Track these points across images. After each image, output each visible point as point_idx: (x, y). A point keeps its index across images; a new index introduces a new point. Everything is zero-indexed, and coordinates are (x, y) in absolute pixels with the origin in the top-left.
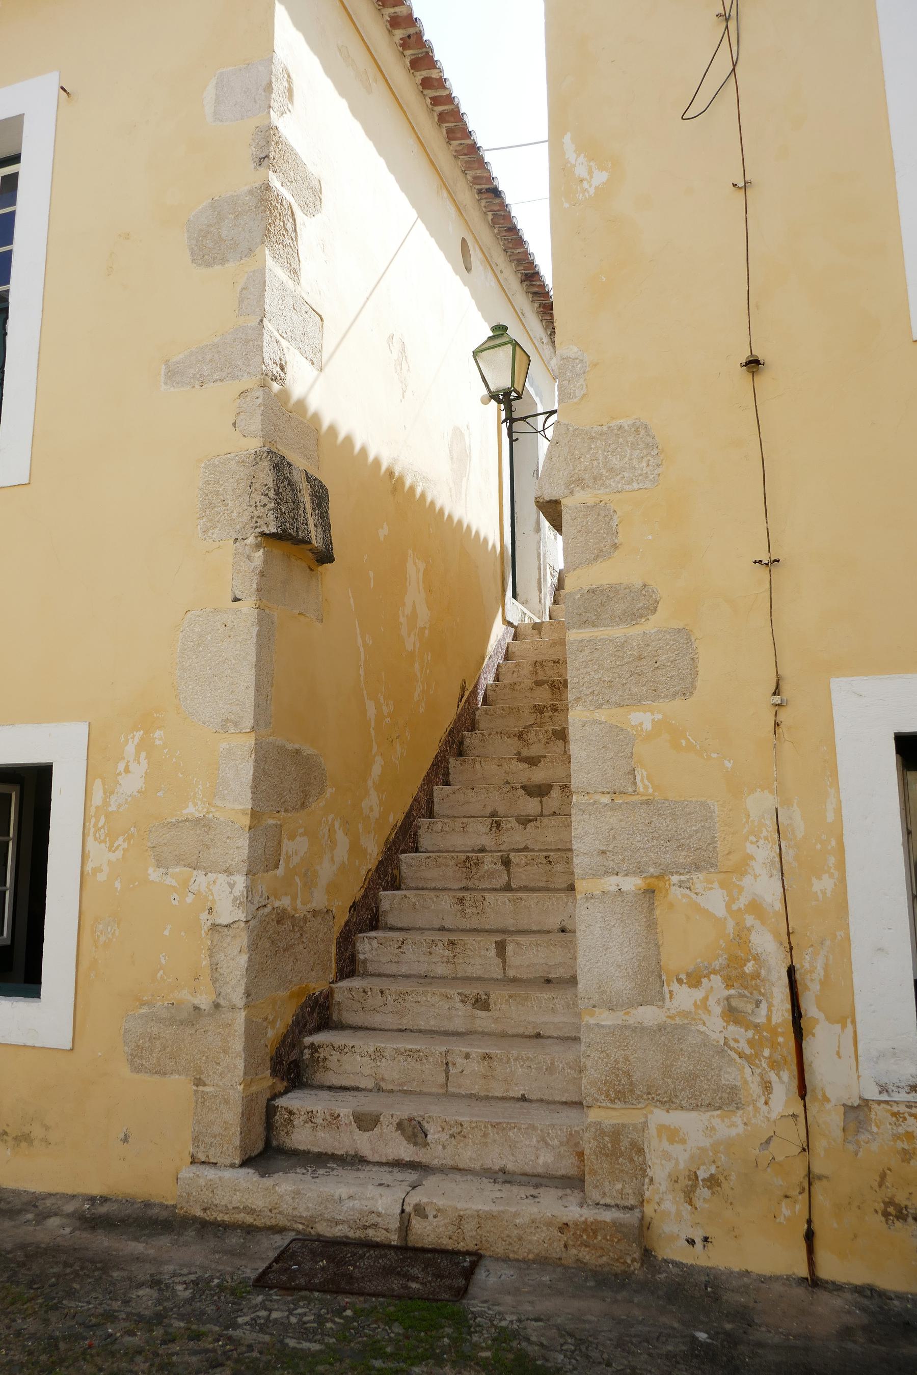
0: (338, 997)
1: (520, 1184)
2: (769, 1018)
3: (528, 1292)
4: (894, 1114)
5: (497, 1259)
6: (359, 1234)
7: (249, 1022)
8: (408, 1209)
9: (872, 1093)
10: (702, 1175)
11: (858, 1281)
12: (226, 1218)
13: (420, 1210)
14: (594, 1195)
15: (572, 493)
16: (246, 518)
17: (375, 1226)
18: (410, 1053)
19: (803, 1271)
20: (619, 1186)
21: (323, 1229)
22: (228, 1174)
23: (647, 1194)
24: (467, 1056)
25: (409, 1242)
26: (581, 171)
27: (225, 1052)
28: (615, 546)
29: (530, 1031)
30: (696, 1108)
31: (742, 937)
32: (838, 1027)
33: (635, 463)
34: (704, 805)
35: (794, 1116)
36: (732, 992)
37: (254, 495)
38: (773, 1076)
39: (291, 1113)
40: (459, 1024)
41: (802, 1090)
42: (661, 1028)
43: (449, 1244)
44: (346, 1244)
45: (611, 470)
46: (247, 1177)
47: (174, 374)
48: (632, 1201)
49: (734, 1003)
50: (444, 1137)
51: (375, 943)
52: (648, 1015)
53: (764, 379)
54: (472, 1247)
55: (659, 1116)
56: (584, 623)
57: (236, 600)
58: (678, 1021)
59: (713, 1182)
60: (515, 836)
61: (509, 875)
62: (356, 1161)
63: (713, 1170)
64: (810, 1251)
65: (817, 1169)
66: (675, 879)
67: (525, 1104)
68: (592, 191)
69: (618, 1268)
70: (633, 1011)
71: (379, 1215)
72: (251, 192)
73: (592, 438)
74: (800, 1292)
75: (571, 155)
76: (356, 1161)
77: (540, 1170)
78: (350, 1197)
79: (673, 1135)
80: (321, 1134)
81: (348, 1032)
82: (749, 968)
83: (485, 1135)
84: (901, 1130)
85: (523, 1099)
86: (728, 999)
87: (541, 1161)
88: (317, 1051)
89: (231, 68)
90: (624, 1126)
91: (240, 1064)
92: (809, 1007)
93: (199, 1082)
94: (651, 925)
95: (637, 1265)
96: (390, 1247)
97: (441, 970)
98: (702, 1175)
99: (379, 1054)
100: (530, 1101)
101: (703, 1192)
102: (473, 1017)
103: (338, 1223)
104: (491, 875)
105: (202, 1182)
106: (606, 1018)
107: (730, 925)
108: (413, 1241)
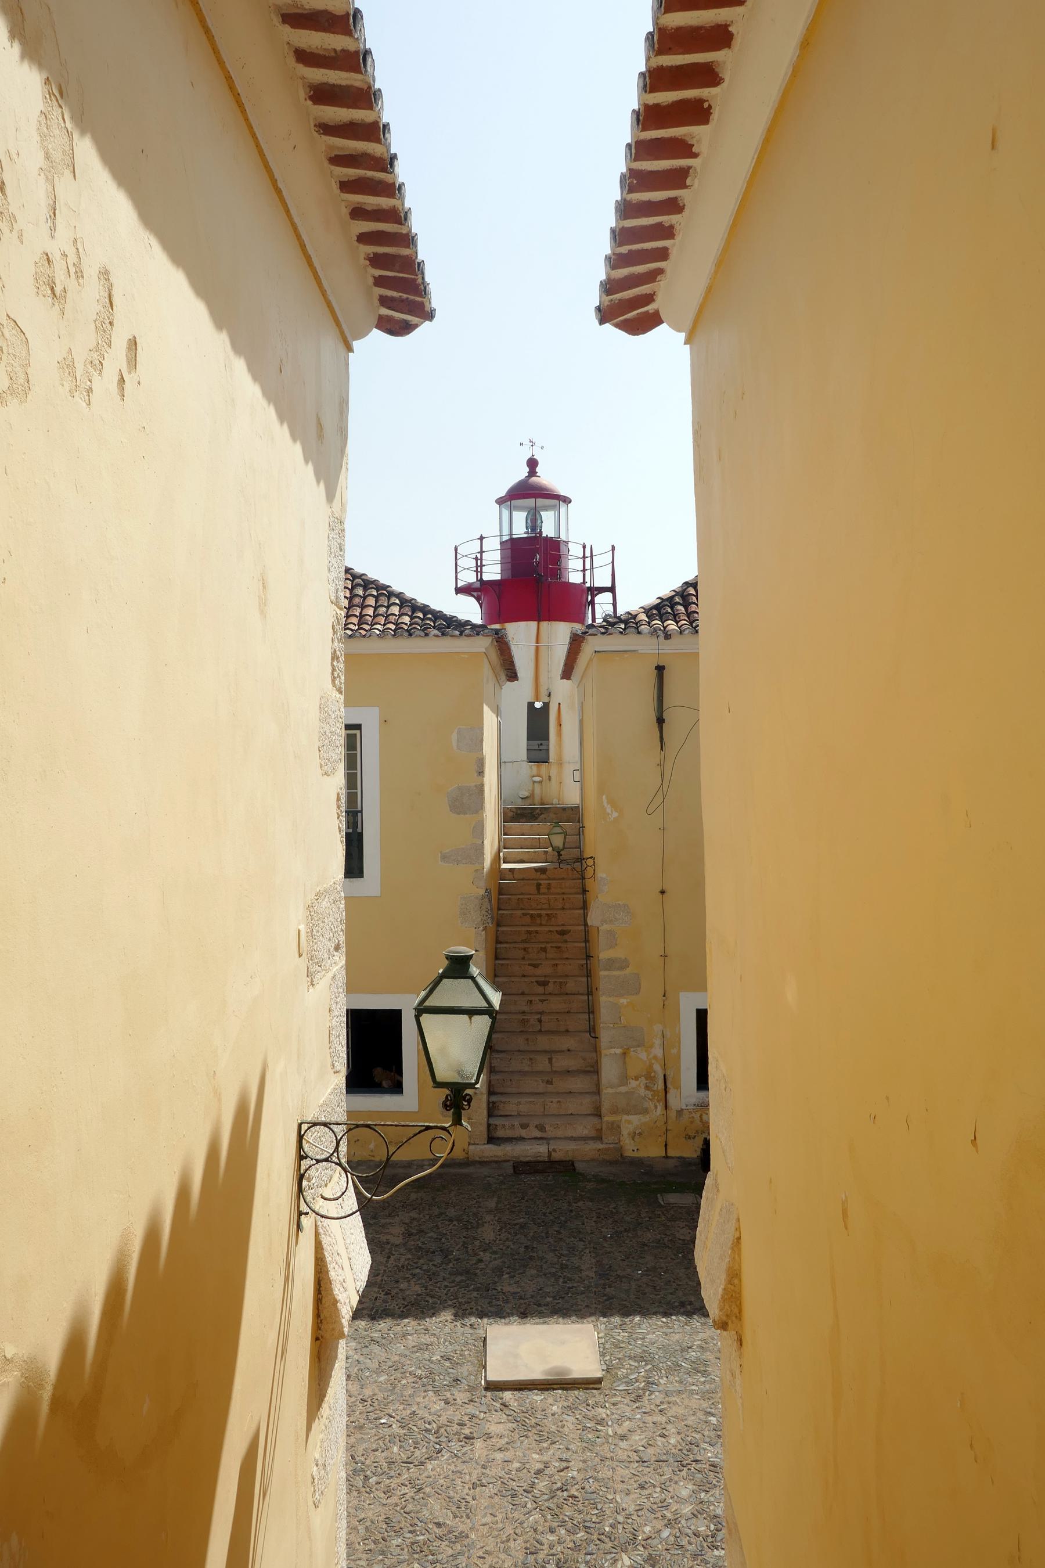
2: (657, 1088)
4: (690, 1112)
5: (579, 1161)
6: (535, 1159)
9: (684, 1107)
10: (637, 1132)
12: (488, 1160)
13: (554, 1150)
14: (605, 1140)
15: (602, 924)
16: (479, 919)
17: (540, 1156)
18: (530, 1102)
19: (664, 1155)
20: (613, 1137)
21: (522, 1159)
22: (482, 1147)
23: (621, 1139)
24: (552, 1102)
25: (551, 1158)
26: (609, 810)
28: (616, 945)
29: (568, 1091)
30: (636, 1114)
31: (651, 1066)
32: (676, 1090)
33: (624, 917)
35: (663, 1115)
36: (648, 1081)
37: (482, 911)
38: (658, 1104)
39: (496, 1126)
40: (541, 1090)
41: (666, 1107)
42: (627, 1093)
43: (564, 1159)
44: (531, 1162)
47: (445, 858)
48: (617, 1142)
49: (647, 1084)
50: (552, 1129)
51: (499, 1060)
52: (623, 1089)
53: (665, 895)
54: (571, 1158)
55: (625, 1117)
56: (606, 970)
58: (631, 1090)
59: (640, 1134)
60: (540, 1007)
61: (541, 1026)
62: (522, 1139)
63: (640, 1131)
64: (666, 1149)
65: (669, 1128)
66: (632, 1049)
67: (572, 1116)
68: (612, 819)
70: (618, 1088)
71: (541, 1153)
72: (476, 786)
75: (605, 804)
76: (522, 1139)
77: (583, 1136)
78: (531, 1149)
79: (630, 1122)
80: (508, 1131)
81: (499, 1095)
82: (652, 1075)
84: (691, 1116)
85: (571, 1114)
86: (646, 1083)
87: (584, 1133)
88: (495, 1104)
89: (464, 727)
90: (615, 1121)
92: (669, 1085)
94: (625, 1063)
95: (620, 1158)
96: (545, 1162)
97: (527, 1069)
98: (637, 1132)
99: (519, 1103)
101: (637, 1137)
102: (546, 1087)
105: (478, 1150)
106: (610, 1091)
107: (648, 1062)
108: (552, 1159)
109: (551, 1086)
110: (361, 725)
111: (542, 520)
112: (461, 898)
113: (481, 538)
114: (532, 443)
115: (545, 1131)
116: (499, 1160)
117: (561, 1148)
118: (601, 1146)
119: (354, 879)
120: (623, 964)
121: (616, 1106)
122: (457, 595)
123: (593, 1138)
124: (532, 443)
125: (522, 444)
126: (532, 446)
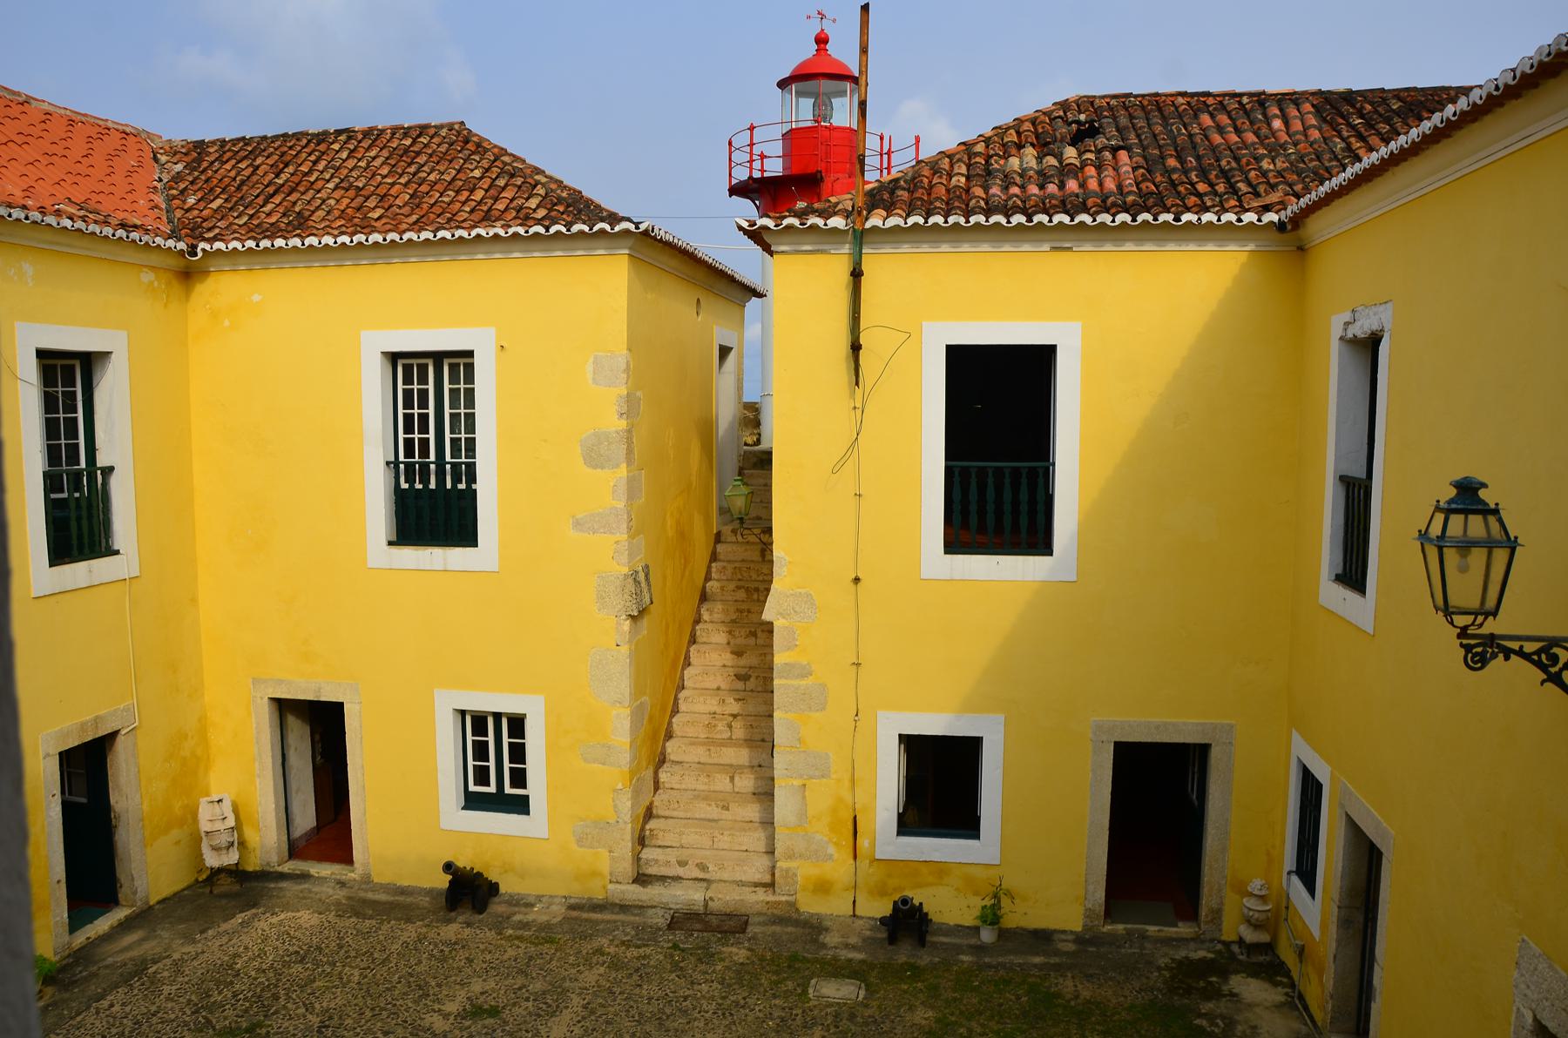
0: (656, 804)
1: (749, 886)
3: (759, 924)
7: (632, 827)
8: (707, 898)
11: (868, 915)
13: (711, 899)
17: (693, 904)
27: (623, 840)
34: (826, 754)
45: (795, 612)
46: (636, 888)
47: (578, 524)
51: (669, 774)
57: (618, 645)
69: (787, 915)
73: (788, 597)
74: (850, 920)
76: (677, 878)
81: (662, 820)
83: (734, 868)
90: (790, 868)
91: (630, 844)
93: (610, 852)
94: (804, 798)
100: (750, 852)
103: (678, 904)
104: (721, 732)
109: (727, 812)
110: (473, 351)
111: (832, 107)
112: (598, 577)
113: (752, 128)
114: (822, 16)
115: (708, 872)
116: (645, 905)
117: (720, 896)
118: (771, 898)
119: (447, 548)
120: (805, 672)
121: (792, 850)
122: (730, 196)
123: (764, 885)
124: (822, 16)
125: (809, 17)
126: (822, 19)
